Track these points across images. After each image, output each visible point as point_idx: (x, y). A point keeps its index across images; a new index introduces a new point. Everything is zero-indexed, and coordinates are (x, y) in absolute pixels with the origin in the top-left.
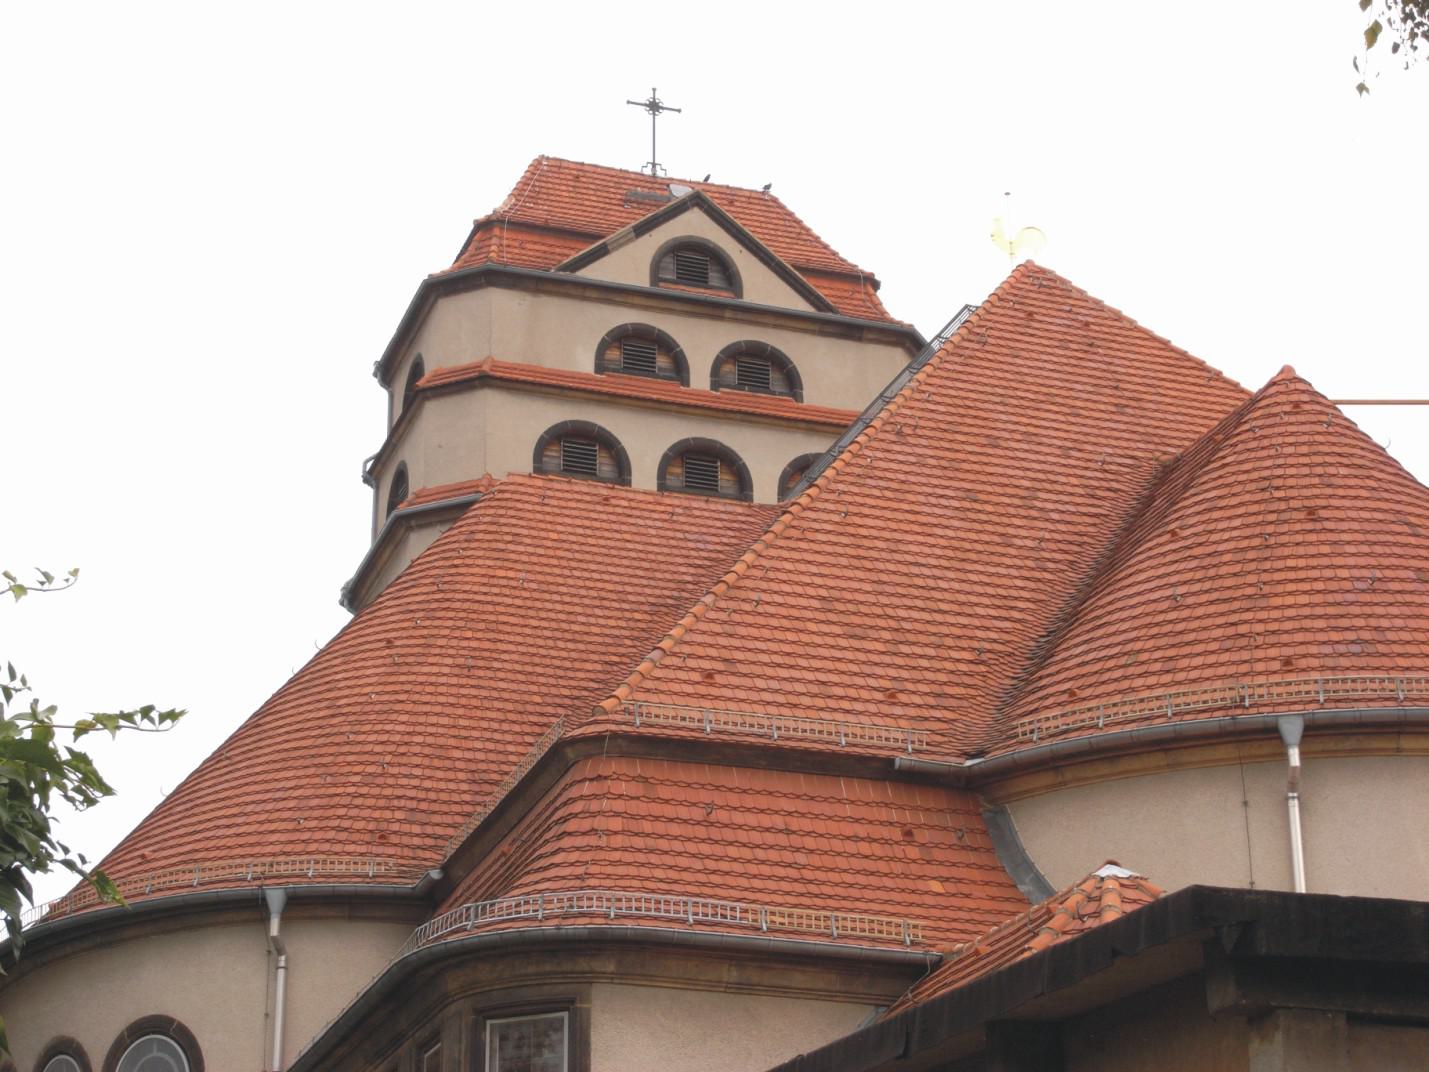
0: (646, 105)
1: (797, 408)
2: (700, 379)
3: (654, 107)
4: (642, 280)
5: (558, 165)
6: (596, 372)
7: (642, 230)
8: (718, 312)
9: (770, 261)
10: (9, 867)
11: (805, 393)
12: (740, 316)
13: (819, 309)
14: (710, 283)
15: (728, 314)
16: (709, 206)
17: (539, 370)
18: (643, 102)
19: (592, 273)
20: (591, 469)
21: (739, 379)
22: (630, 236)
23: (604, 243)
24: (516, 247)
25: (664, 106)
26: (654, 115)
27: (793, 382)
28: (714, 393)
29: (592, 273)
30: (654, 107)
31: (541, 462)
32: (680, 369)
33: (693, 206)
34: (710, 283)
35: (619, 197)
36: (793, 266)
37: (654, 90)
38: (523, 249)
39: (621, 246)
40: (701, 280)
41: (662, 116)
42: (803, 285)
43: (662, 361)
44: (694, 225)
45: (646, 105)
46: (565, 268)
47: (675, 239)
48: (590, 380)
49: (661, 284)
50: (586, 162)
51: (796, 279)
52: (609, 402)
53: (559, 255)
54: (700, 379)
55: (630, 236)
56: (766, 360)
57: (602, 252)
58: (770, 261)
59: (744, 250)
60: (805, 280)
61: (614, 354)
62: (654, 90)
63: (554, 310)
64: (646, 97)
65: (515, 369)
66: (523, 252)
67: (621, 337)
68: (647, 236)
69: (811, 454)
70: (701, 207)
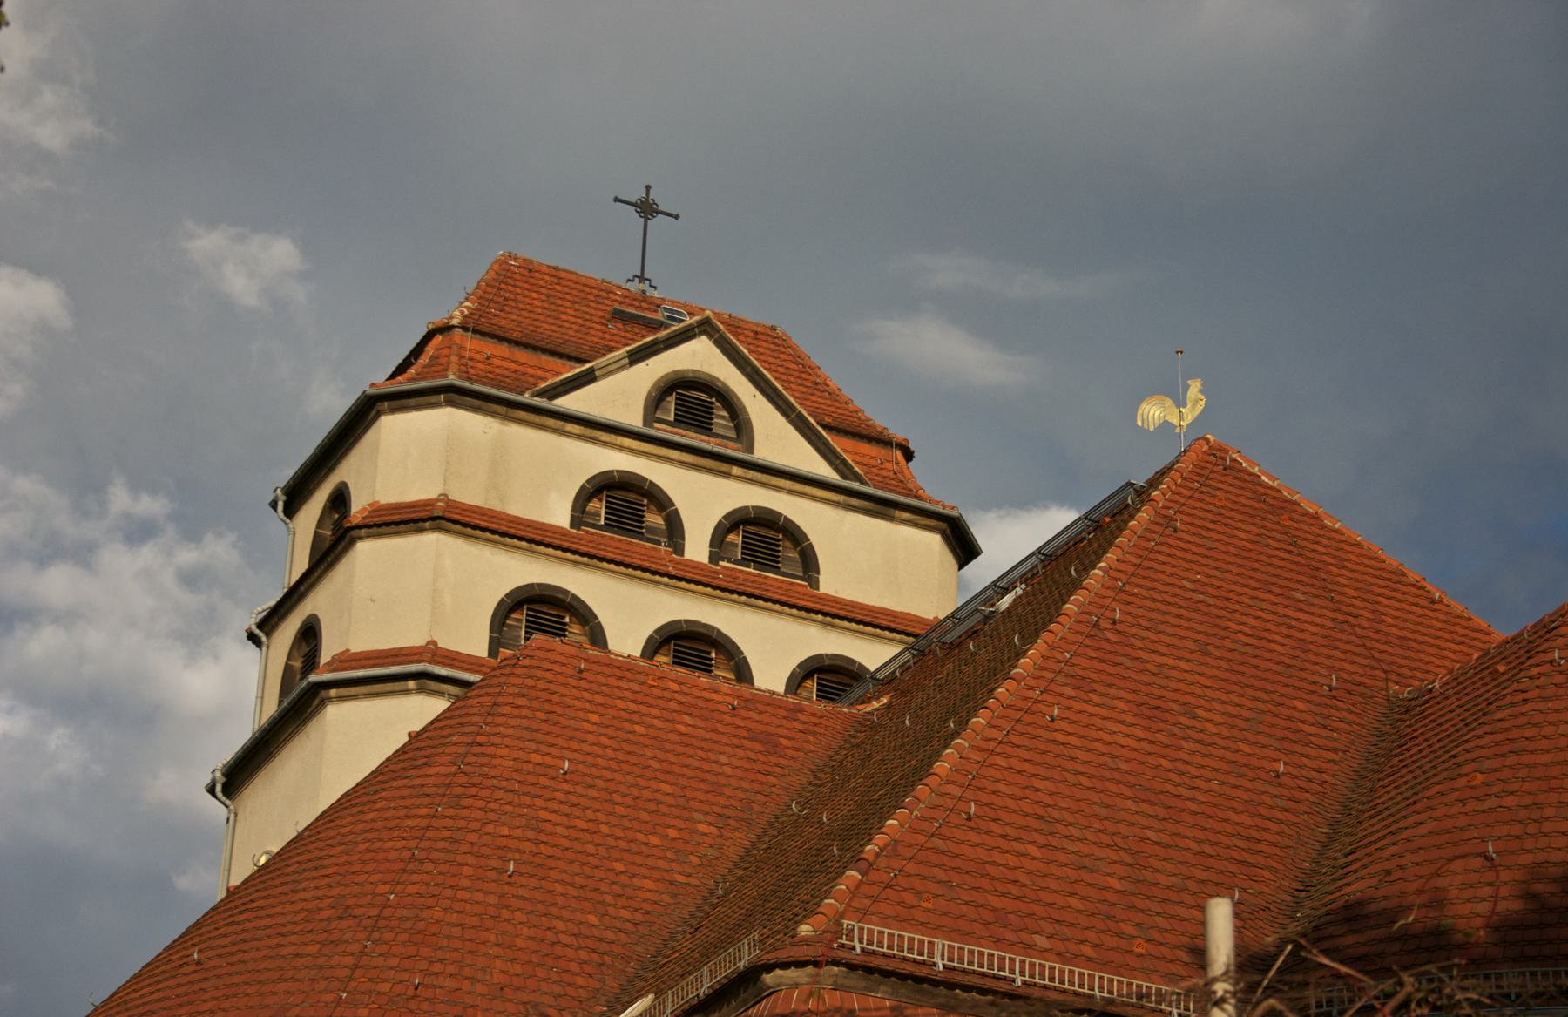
0: (659, 212)
1: (813, 596)
2: (697, 548)
3: (647, 209)
4: (634, 418)
5: (529, 268)
6: (572, 526)
7: (637, 357)
8: (724, 467)
9: (789, 412)
10: (659, 993)
11: (821, 578)
12: (751, 474)
13: (844, 477)
14: (715, 431)
15: (736, 470)
16: (721, 335)
17: (503, 516)
18: (633, 200)
19: (568, 402)
20: (823, 680)
21: (743, 553)
22: (623, 362)
23: (592, 367)
24: (480, 362)
25: (661, 208)
26: (646, 219)
27: (809, 563)
28: (575, 531)
29: (568, 402)
30: (647, 209)
31: (500, 632)
32: (675, 530)
33: (701, 333)
34: (715, 431)
35: (601, 314)
36: (818, 423)
37: (648, 188)
38: (489, 364)
39: (611, 373)
40: (705, 427)
41: (657, 222)
42: (826, 444)
43: (654, 519)
44: (699, 356)
45: (659, 212)
46: (540, 394)
47: (676, 372)
48: (565, 535)
49: (656, 425)
50: (562, 266)
51: (820, 437)
52: (588, 565)
53: (532, 376)
54: (697, 548)
55: (623, 362)
56: (644, 495)
57: (588, 378)
58: (789, 412)
59: (758, 394)
60: (829, 439)
61: (598, 507)
62: (648, 188)
63: (524, 438)
64: (637, 194)
65: (475, 512)
66: (489, 368)
67: (606, 486)
68: (642, 365)
69: (827, 655)
70: (710, 337)
